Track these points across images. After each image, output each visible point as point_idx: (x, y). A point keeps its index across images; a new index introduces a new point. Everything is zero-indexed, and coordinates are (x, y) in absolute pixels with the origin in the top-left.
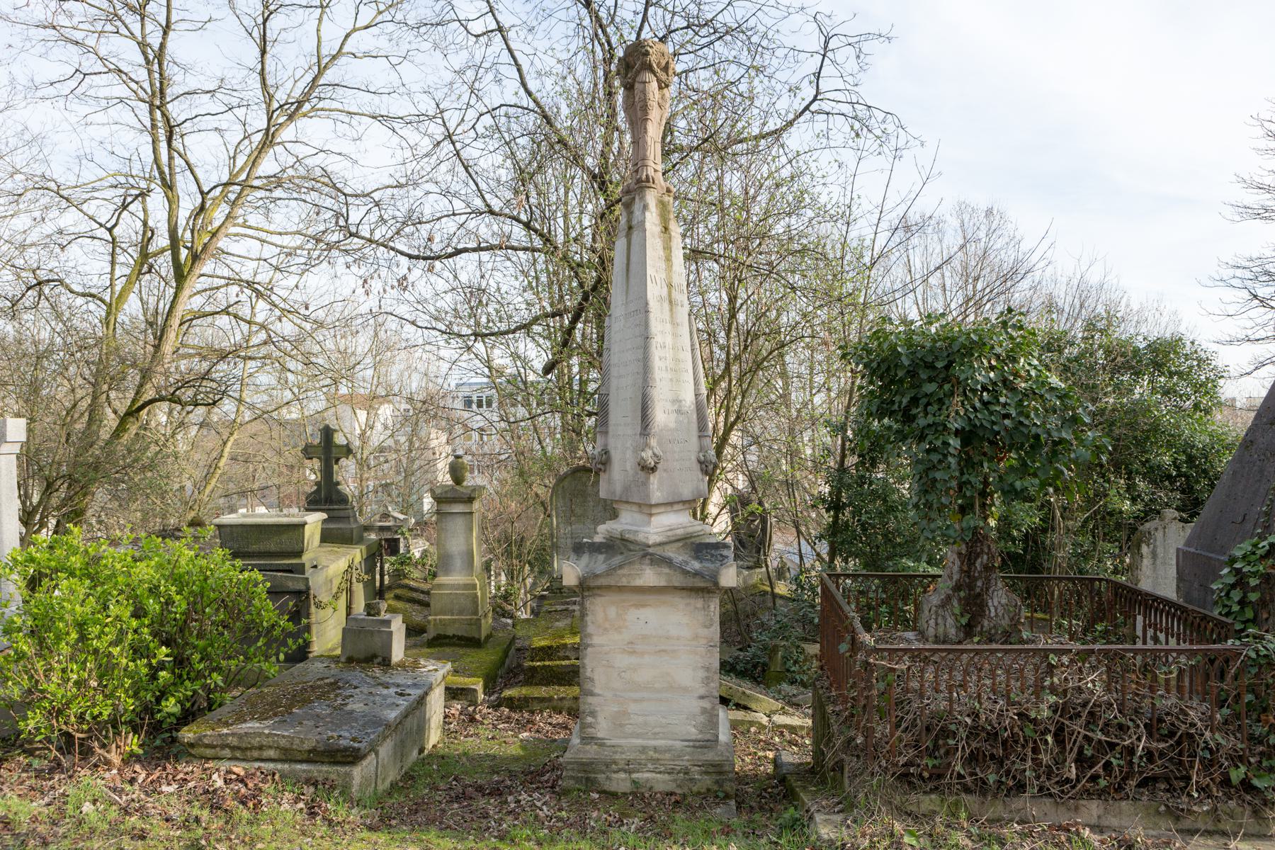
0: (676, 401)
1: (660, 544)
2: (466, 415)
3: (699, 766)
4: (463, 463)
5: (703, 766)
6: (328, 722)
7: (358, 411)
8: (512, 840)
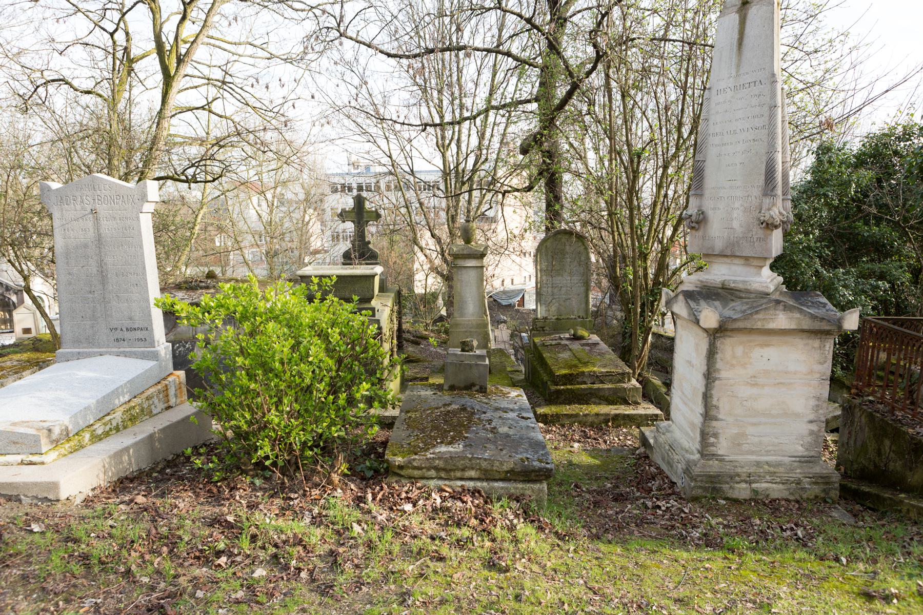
5: (813, 477)
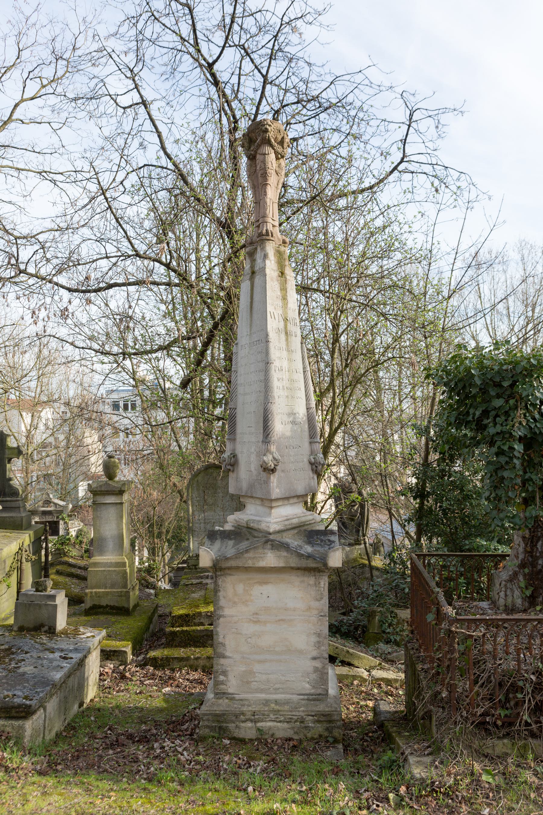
0: (292, 414)
1: (279, 532)
2: (115, 418)
3: (313, 716)
4: (115, 462)
5: (315, 715)
6: (4, 683)
7: (24, 414)
8: (159, 782)
